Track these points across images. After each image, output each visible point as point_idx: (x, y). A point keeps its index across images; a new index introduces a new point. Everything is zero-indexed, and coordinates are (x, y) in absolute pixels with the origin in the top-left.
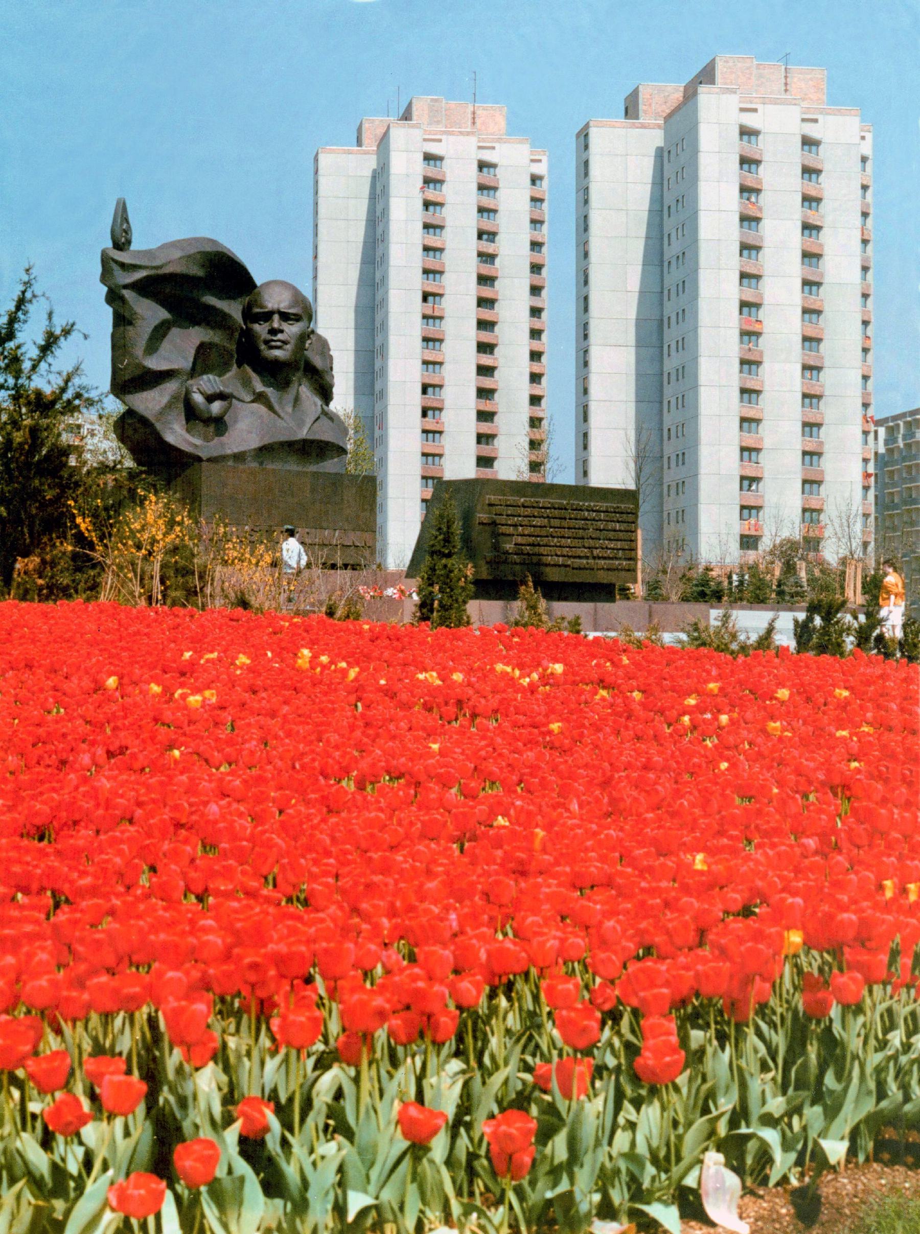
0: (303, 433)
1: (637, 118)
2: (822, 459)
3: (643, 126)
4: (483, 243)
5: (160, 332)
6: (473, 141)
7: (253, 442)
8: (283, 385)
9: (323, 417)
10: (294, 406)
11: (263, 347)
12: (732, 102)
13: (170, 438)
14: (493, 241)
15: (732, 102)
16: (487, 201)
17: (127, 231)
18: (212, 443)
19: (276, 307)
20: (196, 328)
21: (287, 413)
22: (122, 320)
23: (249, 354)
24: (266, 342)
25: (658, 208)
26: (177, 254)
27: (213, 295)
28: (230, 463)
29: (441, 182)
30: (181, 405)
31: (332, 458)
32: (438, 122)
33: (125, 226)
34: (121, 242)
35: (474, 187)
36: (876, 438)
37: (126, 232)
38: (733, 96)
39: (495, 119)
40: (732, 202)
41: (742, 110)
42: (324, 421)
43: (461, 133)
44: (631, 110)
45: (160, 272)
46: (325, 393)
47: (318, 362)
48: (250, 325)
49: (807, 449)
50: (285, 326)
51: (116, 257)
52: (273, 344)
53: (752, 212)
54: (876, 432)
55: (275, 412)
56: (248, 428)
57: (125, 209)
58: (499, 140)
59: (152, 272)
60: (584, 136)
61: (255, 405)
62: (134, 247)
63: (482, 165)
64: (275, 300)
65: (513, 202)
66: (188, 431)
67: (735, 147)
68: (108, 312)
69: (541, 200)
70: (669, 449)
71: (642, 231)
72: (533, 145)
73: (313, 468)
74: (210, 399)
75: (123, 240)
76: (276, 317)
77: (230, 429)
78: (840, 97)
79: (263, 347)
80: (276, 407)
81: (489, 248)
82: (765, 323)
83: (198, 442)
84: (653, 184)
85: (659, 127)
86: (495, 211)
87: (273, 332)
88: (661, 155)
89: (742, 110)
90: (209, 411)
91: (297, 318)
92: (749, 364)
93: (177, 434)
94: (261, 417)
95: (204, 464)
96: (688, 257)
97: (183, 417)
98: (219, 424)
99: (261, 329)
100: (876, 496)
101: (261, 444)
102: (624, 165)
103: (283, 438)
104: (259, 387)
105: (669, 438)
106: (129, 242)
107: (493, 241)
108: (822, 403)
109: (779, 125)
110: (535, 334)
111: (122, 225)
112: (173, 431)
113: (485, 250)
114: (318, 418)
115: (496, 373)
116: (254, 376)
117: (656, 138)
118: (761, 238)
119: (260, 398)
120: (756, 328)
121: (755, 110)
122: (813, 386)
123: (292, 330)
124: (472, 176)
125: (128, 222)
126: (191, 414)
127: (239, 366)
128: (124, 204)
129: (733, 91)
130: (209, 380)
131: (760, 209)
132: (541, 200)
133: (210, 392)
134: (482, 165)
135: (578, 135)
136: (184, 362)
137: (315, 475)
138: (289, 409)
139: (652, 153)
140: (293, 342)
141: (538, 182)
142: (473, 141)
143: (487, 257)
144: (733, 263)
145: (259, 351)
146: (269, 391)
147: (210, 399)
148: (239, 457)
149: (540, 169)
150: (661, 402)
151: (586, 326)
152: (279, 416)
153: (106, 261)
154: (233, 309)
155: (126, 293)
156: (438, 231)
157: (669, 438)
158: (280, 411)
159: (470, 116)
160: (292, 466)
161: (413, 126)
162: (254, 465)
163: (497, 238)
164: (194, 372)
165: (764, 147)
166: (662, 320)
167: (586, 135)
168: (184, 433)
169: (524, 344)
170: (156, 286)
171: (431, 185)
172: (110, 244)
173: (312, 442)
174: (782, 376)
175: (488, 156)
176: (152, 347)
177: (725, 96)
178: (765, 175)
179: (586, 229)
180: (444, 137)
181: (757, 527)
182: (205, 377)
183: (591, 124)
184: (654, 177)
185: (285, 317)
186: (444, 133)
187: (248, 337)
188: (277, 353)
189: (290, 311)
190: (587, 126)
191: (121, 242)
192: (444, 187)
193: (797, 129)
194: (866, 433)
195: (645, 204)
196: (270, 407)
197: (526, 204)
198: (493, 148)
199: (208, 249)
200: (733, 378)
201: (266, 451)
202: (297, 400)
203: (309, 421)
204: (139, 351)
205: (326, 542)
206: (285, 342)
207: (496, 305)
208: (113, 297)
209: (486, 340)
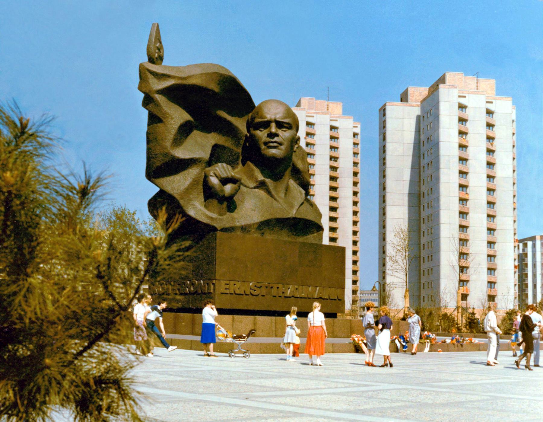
0: (293, 213)
1: (407, 101)
2: (496, 259)
3: (411, 106)
4: (332, 162)
5: (185, 130)
6: (328, 117)
7: (256, 218)
8: (277, 177)
9: (305, 202)
10: (286, 194)
11: (263, 147)
12: (455, 92)
13: (191, 213)
14: (336, 161)
15: (455, 92)
16: (334, 144)
17: (160, 49)
18: (225, 217)
19: (273, 117)
20: (213, 134)
21: (281, 198)
22: (154, 119)
23: (252, 153)
24: (266, 144)
25: (417, 142)
26: (198, 71)
27: (225, 111)
28: (239, 233)
29: (314, 135)
30: (201, 187)
31: (313, 233)
32: (312, 109)
33: (158, 45)
34: (155, 57)
35: (328, 137)
36: (519, 248)
37: (159, 49)
38: (455, 89)
39: (337, 108)
40: (456, 139)
41: (460, 97)
42: (306, 205)
43: (323, 113)
44: (404, 98)
45: (186, 82)
46: (306, 186)
47: (300, 165)
48: (253, 132)
49: (490, 254)
50: (280, 132)
51: (150, 68)
52: (271, 144)
53: (464, 143)
54: (518, 246)
55: (272, 196)
56: (252, 207)
57: (158, 39)
58: (339, 117)
59: (180, 82)
60: (383, 111)
61: (256, 190)
62: (165, 63)
63: (332, 128)
64: (273, 113)
65: (346, 145)
66: (205, 206)
67: (456, 113)
68: (145, 113)
69: (358, 144)
70: (424, 253)
71: (411, 153)
72: (354, 120)
73: (301, 239)
74: (225, 181)
75: (156, 55)
76: (273, 125)
77: (239, 208)
78: (501, 92)
79: (263, 147)
80: (273, 193)
81: (335, 164)
82: (470, 195)
83: (214, 216)
84: (416, 131)
85: (418, 106)
86: (337, 148)
87: (272, 135)
88: (419, 119)
89: (460, 97)
90: (223, 191)
91: (289, 127)
92: (463, 214)
93: (198, 209)
94: (261, 199)
95: (219, 234)
96: (435, 164)
97: (202, 196)
98: (230, 204)
99: (262, 135)
100: (519, 275)
101: (262, 219)
102: (402, 123)
103: (278, 216)
104: (261, 177)
105: (424, 249)
106: (161, 58)
107: (336, 161)
108: (495, 232)
109: (476, 105)
110: (355, 203)
111: (155, 43)
112: (195, 207)
113: (333, 165)
114: (303, 203)
115: (338, 220)
116: (255, 168)
117: (417, 111)
118: (468, 155)
119: (262, 185)
120: (466, 197)
121: (465, 97)
122: (492, 224)
123: (284, 135)
124: (328, 133)
125: (161, 43)
126: (209, 193)
127: (244, 164)
128: (158, 26)
129: (455, 87)
130: (223, 167)
131: (467, 142)
132: (358, 144)
133: (224, 175)
134: (332, 128)
135: (380, 110)
136: (205, 154)
137: (304, 244)
138: (283, 195)
139: (415, 117)
140: (286, 143)
141: (356, 136)
142: (328, 117)
143: (334, 169)
144: (456, 166)
145: (259, 149)
146: (268, 181)
147: (225, 181)
148: (244, 229)
149: (358, 130)
150: (420, 232)
151: (384, 197)
152: (276, 199)
153: (143, 73)
154: (240, 124)
155: (158, 97)
156: (312, 156)
157: (424, 249)
158: (276, 196)
159: (326, 107)
160: (284, 236)
161: (302, 110)
162: (257, 235)
163: (338, 160)
164: (210, 163)
165: (469, 114)
166: (420, 194)
167: (384, 110)
168: (202, 208)
169: (350, 208)
170: (183, 93)
171: (309, 136)
172: (146, 59)
173: (300, 219)
174: (478, 220)
175: (334, 124)
176: (178, 141)
177: (451, 90)
178: (469, 127)
179: (384, 151)
180: (315, 115)
181: (467, 290)
182: (220, 164)
183: (387, 104)
184: (416, 128)
185: (280, 125)
186: (315, 113)
187: (252, 141)
188: (273, 151)
189: (285, 121)
190: (385, 105)
191: (155, 57)
192: (315, 137)
193: (484, 106)
194: (515, 247)
195: (412, 141)
196: (268, 192)
197: (352, 146)
198: (337, 120)
199: (222, 72)
200: (456, 220)
201: (265, 225)
202: (287, 189)
203: (297, 205)
204: (168, 144)
205: (310, 296)
206: (280, 144)
207: (338, 190)
208: (148, 101)
209: (333, 206)
